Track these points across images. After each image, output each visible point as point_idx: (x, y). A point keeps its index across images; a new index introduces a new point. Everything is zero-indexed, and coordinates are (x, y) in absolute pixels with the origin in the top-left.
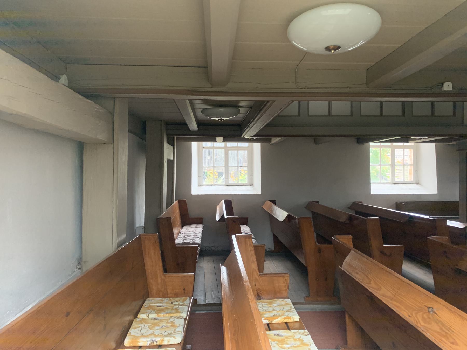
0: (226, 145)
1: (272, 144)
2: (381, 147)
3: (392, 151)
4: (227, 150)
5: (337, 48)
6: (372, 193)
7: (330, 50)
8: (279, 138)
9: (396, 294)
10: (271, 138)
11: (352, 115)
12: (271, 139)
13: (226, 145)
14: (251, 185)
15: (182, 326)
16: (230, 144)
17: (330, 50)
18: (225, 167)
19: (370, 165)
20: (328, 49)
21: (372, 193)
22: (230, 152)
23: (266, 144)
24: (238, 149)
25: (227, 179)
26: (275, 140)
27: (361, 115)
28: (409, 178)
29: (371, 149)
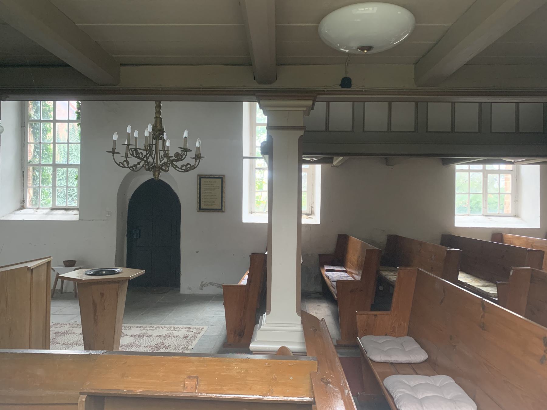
0: (484, 168)
1: (334, 166)
2: (469, 171)
3: (484, 176)
4: (486, 173)
5: (369, 48)
6: (244, 221)
7: (363, 50)
8: (341, 158)
9: (391, 333)
10: (333, 158)
11: (353, 130)
12: (332, 158)
13: (484, 168)
14: (516, 216)
15: (380, 359)
16: (489, 167)
17: (363, 50)
18: (483, 193)
19: (302, 191)
20: (362, 48)
21: (244, 221)
22: (490, 176)
23: (327, 166)
24: (499, 172)
25: (54, 200)
26: (337, 160)
27: (491, 132)
28: (509, 209)
29: (457, 174)
